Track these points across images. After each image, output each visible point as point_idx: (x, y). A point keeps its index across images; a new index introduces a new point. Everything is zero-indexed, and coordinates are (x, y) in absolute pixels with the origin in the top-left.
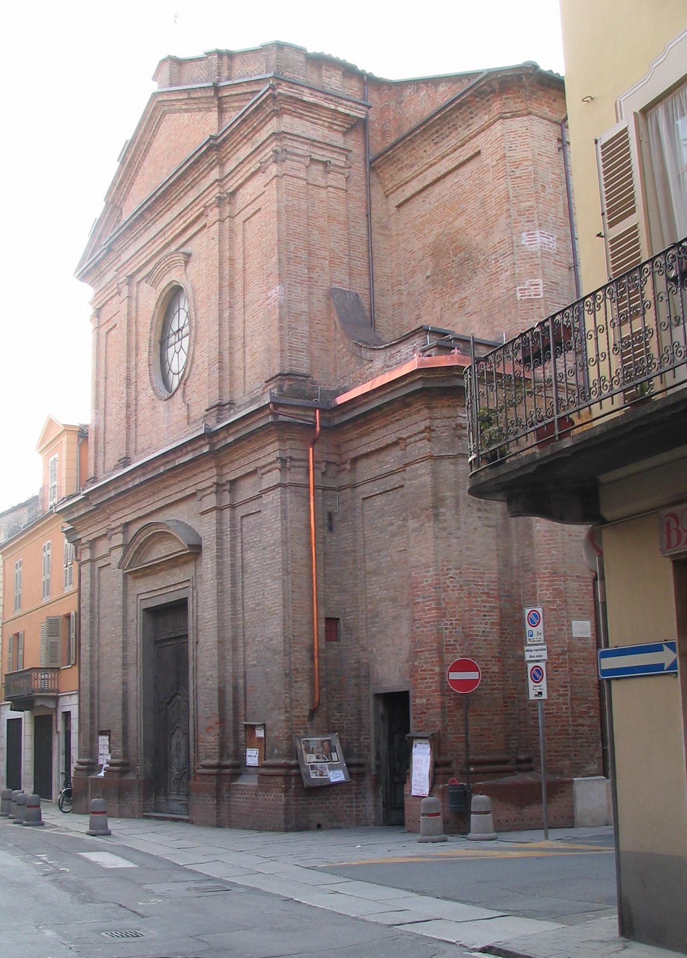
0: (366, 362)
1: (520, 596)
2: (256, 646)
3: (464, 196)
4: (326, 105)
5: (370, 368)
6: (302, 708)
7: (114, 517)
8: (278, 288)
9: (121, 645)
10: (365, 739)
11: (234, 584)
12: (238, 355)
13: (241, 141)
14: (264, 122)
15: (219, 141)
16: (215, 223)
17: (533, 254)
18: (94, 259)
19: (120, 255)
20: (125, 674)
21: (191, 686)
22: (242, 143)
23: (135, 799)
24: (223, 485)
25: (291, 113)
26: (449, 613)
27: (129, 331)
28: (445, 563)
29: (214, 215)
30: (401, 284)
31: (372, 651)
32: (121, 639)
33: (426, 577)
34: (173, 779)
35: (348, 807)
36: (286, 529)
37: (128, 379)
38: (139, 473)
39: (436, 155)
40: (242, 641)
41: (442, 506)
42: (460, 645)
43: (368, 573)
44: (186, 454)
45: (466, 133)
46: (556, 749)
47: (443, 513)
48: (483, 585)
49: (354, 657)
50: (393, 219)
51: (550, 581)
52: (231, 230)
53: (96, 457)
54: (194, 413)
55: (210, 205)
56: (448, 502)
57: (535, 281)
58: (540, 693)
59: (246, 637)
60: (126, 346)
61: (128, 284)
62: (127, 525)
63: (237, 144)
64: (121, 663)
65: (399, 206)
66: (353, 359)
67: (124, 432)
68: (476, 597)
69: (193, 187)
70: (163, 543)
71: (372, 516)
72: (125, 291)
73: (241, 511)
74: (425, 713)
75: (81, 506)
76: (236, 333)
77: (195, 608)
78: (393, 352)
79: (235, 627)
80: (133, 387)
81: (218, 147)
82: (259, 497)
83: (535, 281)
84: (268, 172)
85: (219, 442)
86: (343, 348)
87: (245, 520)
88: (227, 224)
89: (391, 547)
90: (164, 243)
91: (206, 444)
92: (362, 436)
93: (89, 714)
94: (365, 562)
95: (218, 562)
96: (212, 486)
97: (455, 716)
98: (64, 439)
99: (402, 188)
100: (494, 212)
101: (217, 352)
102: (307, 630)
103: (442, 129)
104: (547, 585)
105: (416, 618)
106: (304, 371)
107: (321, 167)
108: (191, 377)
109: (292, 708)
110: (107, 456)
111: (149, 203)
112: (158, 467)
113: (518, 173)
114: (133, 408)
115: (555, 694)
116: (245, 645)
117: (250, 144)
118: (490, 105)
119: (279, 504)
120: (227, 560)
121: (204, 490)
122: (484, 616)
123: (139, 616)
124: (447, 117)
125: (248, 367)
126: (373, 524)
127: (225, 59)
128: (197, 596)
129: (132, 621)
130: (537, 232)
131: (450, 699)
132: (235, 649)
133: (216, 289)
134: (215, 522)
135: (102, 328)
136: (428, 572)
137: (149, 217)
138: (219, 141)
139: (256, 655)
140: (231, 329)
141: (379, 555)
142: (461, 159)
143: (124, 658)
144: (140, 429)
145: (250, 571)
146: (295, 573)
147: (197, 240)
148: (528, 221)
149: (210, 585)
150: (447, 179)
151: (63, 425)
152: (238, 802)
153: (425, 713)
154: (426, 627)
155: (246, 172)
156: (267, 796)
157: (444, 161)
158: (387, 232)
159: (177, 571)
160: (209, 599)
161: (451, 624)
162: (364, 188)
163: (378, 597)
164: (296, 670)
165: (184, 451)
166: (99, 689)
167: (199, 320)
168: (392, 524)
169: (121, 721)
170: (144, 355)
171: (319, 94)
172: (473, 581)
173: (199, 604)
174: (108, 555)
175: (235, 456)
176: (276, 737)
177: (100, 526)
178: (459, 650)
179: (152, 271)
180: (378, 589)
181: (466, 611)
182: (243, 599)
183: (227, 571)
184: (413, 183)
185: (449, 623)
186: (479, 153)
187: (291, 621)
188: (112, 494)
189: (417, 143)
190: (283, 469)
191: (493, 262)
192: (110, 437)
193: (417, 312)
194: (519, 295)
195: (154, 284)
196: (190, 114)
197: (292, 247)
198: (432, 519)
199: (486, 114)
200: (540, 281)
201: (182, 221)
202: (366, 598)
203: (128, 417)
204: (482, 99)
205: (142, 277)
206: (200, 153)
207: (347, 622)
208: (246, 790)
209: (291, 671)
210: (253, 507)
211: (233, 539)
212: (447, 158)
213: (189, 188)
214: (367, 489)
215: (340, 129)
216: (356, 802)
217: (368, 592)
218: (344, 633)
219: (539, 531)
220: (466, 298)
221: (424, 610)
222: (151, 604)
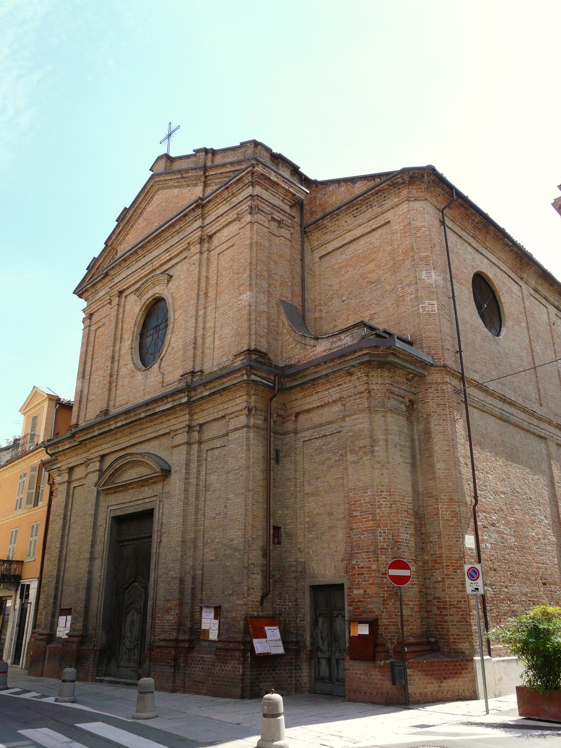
0: (309, 347)
1: (424, 515)
2: (215, 545)
3: (375, 249)
4: (283, 185)
5: (314, 351)
6: (256, 595)
7: (92, 451)
8: (248, 293)
9: (90, 543)
10: (300, 621)
11: (197, 498)
12: (209, 340)
13: (222, 202)
14: (241, 190)
15: (205, 202)
16: (196, 254)
17: (430, 285)
18: (93, 281)
19: (113, 279)
20: (91, 566)
21: (152, 575)
22: (222, 204)
23: (91, 663)
24: (194, 427)
25: (261, 186)
26: (382, 523)
27: (116, 327)
28: (379, 487)
29: (195, 248)
30: (321, 306)
31: (309, 553)
32: (91, 539)
33: (364, 496)
34: (125, 649)
35: (289, 677)
36: (249, 458)
37: (113, 358)
38: (123, 418)
39: (354, 224)
40: (202, 541)
41: (375, 446)
42: (391, 549)
43: (307, 494)
44: (166, 404)
45: (380, 210)
46: (459, 633)
47: (377, 450)
48: (404, 505)
49: (293, 557)
50: (317, 265)
51: (448, 505)
52: (208, 259)
53: (79, 411)
54: (168, 380)
55: (193, 243)
56: (381, 443)
57: (432, 302)
58: (477, 589)
59: (206, 538)
60: (113, 336)
61: (119, 297)
62: (103, 457)
63: (218, 204)
64: (89, 556)
65: (321, 258)
66: (298, 346)
67: (107, 393)
68: (401, 514)
69: (178, 233)
70: (134, 469)
71: (311, 453)
72: (115, 301)
73: (205, 447)
74: (362, 601)
75: (66, 442)
76: (208, 325)
77: (160, 516)
78: (334, 340)
79: (197, 531)
80: (116, 363)
81: (203, 206)
82: (227, 434)
83: (432, 302)
84: (242, 220)
85: (195, 395)
86: (289, 339)
87: (209, 453)
88: (205, 255)
89: (329, 475)
90: (151, 269)
91: (185, 397)
92: (305, 397)
93: (53, 595)
94: (304, 486)
95: (185, 482)
96: (185, 427)
97: (388, 604)
98: (46, 404)
99: (325, 246)
100: (401, 258)
101: (193, 337)
102: (261, 534)
103: (361, 207)
104: (446, 508)
105: (354, 527)
106: (264, 350)
107: (276, 224)
108: (166, 355)
109: (248, 595)
110: (88, 410)
111: (144, 242)
112: (140, 413)
113: (419, 234)
114: (115, 377)
115: (455, 590)
116: (205, 544)
117: (228, 204)
118: (400, 192)
119: (245, 440)
120: (193, 481)
121: (176, 430)
122: (406, 527)
123: (108, 522)
124: (367, 199)
125: (216, 348)
126: (312, 458)
127: (210, 155)
128: (163, 507)
129: (100, 525)
130: (433, 271)
131: (384, 591)
132: (195, 547)
133: (194, 296)
134: (185, 453)
135: (92, 327)
136: (367, 492)
137: (140, 252)
138: (205, 202)
139: (214, 552)
140: (205, 322)
141: (317, 482)
142: (374, 227)
143: (92, 552)
144: (119, 392)
145: (212, 489)
146: (254, 491)
147: (178, 267)
148: (426, 265)
149: (177, 499)
150: (360, 240)
151: (48, 394)
152: (194, 671)
153: (362, 601)
154: (363, 534)
155: (224, 221)
156: (225, 667)
157: (359, 228)
158: (312, 273)
159: (146, 489)
160: (176, 510)
161: (385, 533)
162: (299, 243)
163: (315, 512)
164: (254, 564)
165: (166, 401)
166: (63, 577)
167: (176, 318)
168: (330, 459)
169: (84, 602)
170: (127, 343)
171: (279, 177)
172: (399, 501)
173: (164, 513)
174: (85, 478)
175: (205, 406)
176: (233, 617)
177: (79, 457)
178: (390, 553)
179: (140, 287)
180: (315, 506)
181: (394, 523)
182: (204, 510)
183: (192, 489)
184: (334, 243)
185: (383, 532)
186: (389, 222)
187: (250, 527)
188: (96, 433)
189: (341, 216)
190: (248, 416)
191: (400, 289)
192: (91, 397)
193: (334, 323)
194: (421, 310)
195: (140, 297)
196: (179, 189)
197: (259, 269)
198: (370, 454)
199: (396, 198)
200: (435, 302)
201: (168, 254)
202: (304, 513)
203: (110, 383)
204: (395, 187)
205: (130, 292)
206: (189, 209)
207: (287, 530)
208: (203, 661)
209: (248, 565)
210: (218, 443)
211: (199, 466)
212: (362, 226)
213: (176, 233)
214: (307, 434)
215: (288, 203)
216: (295, 673)
217: (306, 508)
218: (285, 538)
219: (439, 469)
220: (375, 313)
221: (362, 522)
222: (119, 513)
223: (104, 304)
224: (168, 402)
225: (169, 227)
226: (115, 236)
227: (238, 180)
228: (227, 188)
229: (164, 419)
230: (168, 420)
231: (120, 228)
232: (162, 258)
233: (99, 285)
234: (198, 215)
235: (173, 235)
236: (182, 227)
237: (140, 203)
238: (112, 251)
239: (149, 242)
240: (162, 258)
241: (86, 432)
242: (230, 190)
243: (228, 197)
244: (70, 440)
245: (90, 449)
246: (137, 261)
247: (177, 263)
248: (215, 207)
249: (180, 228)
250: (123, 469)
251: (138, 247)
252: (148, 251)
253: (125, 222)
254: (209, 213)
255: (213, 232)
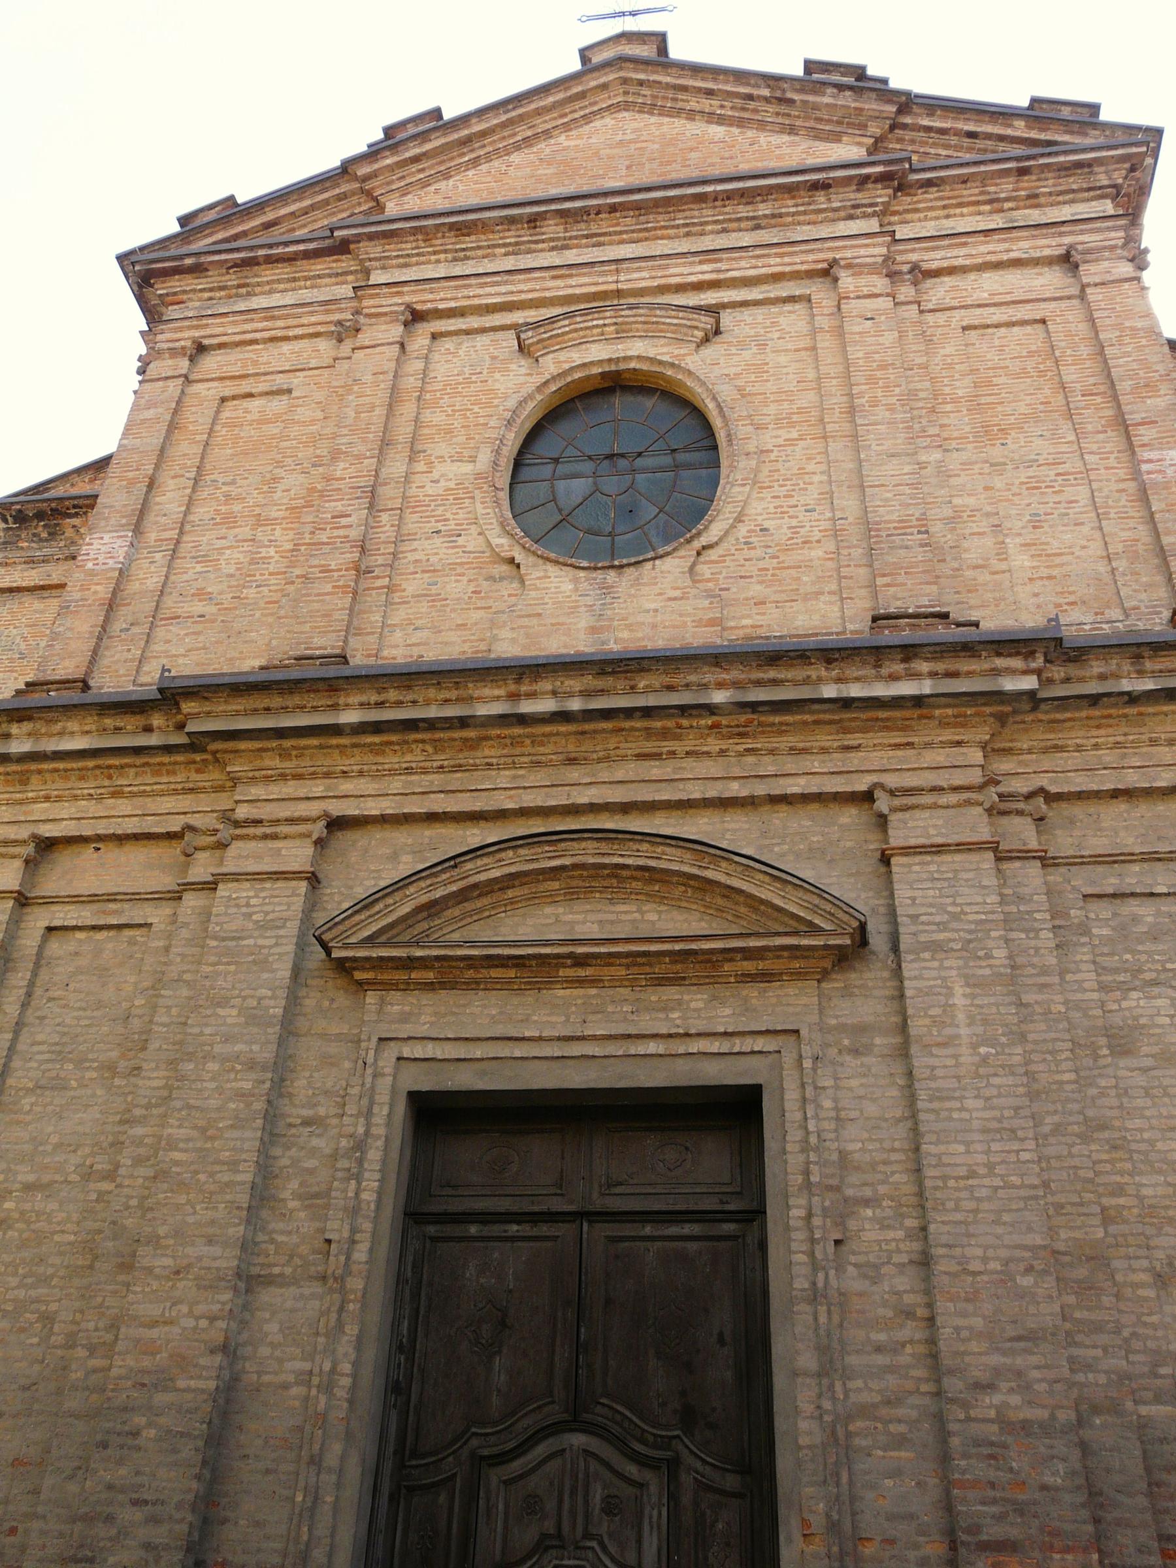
13: (978, 203)
22: (971, 209)
81: (902, 188)
85: (1067, 680)
108: (724, 545)
137: (552, 229)
147: (746, 314)
188: (350, 717)
223: (258, 336)
224: (915, 675)
225: (729, 196)
226: (396, 159)
227: (1079, 165)
228: (1023, 172)
229: (824, 739)
230: (848, 748)
231: (428, 147)
232: (672, 271)
233: (268, 274)
234: (871, 205)
235: (735, 225)
236: (781, 216)
237: (538, 112)
238: (355, 200)
239: (613, 209)
240: (672, 271)
241: (276, 701)
242: (1027, 182)
243: (1007, 199)
244: (109, 722)
245: (235, 781)
246: (516, 249)
247: (744, 304)
248: (944, 207)
249: (773, 216)
250: (510, 893)
251: (553, 207)
252: (587, 237)
253: (456, 136)
254: (909, 216)
255: (934, 265)
